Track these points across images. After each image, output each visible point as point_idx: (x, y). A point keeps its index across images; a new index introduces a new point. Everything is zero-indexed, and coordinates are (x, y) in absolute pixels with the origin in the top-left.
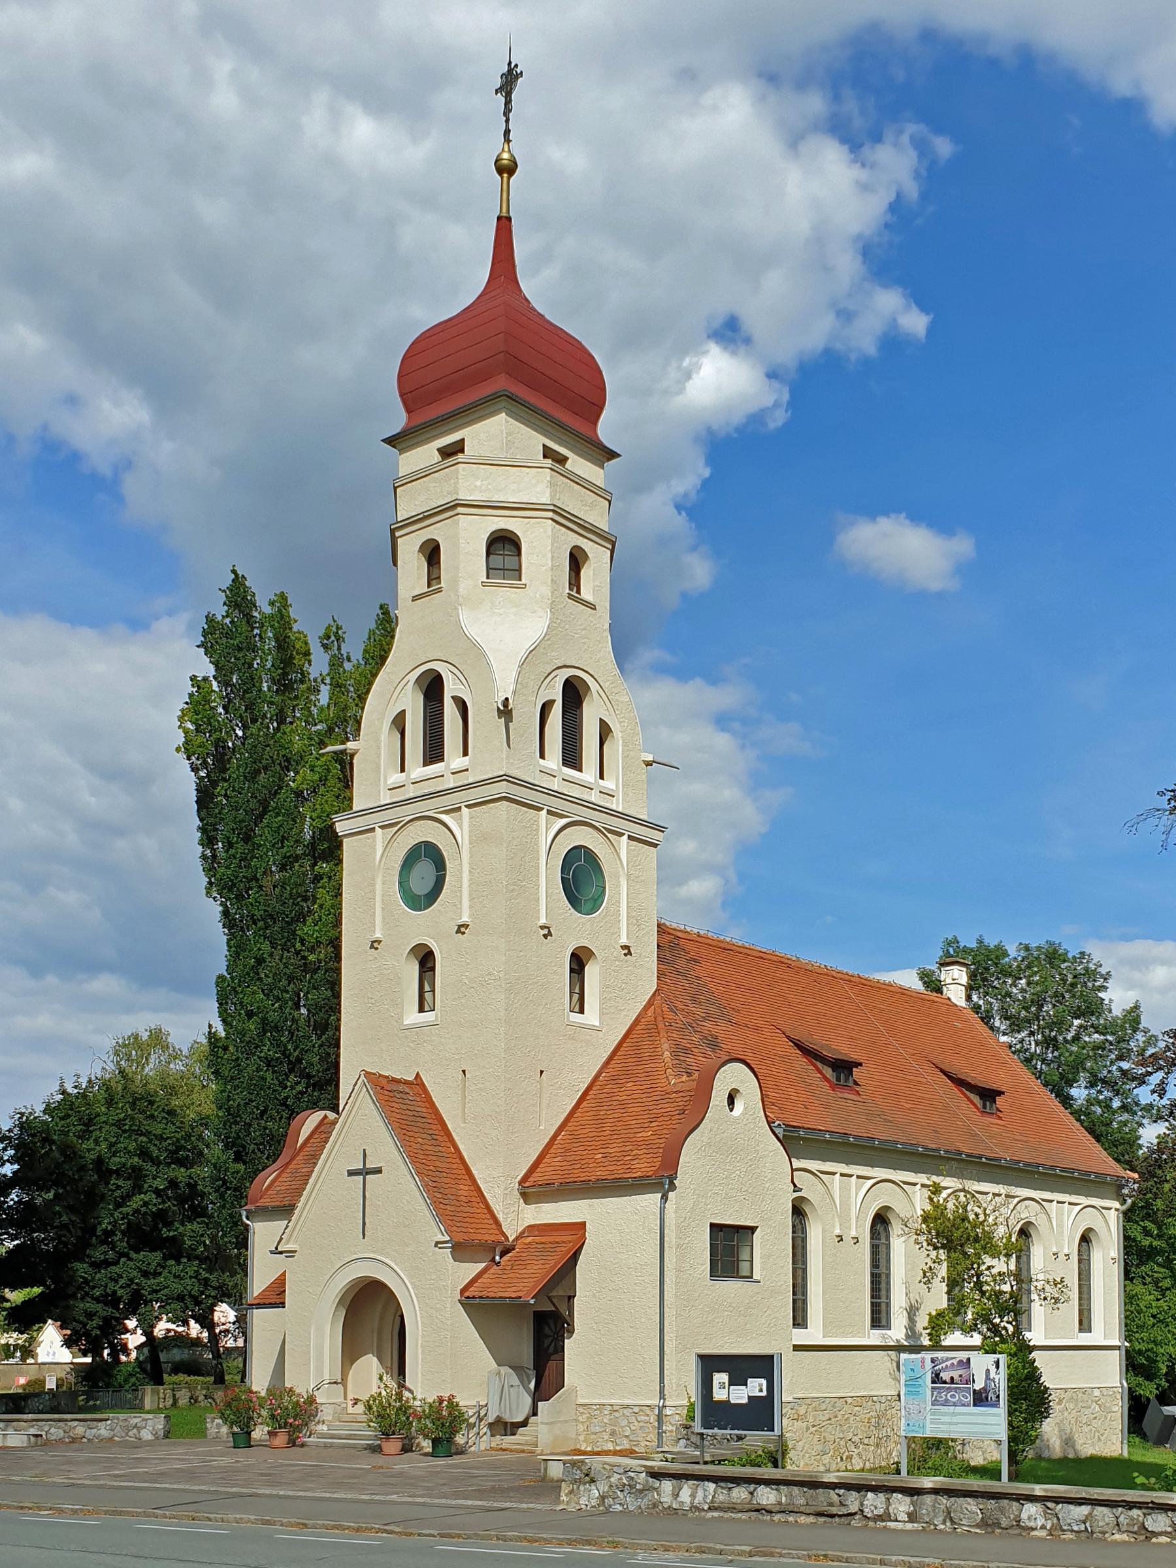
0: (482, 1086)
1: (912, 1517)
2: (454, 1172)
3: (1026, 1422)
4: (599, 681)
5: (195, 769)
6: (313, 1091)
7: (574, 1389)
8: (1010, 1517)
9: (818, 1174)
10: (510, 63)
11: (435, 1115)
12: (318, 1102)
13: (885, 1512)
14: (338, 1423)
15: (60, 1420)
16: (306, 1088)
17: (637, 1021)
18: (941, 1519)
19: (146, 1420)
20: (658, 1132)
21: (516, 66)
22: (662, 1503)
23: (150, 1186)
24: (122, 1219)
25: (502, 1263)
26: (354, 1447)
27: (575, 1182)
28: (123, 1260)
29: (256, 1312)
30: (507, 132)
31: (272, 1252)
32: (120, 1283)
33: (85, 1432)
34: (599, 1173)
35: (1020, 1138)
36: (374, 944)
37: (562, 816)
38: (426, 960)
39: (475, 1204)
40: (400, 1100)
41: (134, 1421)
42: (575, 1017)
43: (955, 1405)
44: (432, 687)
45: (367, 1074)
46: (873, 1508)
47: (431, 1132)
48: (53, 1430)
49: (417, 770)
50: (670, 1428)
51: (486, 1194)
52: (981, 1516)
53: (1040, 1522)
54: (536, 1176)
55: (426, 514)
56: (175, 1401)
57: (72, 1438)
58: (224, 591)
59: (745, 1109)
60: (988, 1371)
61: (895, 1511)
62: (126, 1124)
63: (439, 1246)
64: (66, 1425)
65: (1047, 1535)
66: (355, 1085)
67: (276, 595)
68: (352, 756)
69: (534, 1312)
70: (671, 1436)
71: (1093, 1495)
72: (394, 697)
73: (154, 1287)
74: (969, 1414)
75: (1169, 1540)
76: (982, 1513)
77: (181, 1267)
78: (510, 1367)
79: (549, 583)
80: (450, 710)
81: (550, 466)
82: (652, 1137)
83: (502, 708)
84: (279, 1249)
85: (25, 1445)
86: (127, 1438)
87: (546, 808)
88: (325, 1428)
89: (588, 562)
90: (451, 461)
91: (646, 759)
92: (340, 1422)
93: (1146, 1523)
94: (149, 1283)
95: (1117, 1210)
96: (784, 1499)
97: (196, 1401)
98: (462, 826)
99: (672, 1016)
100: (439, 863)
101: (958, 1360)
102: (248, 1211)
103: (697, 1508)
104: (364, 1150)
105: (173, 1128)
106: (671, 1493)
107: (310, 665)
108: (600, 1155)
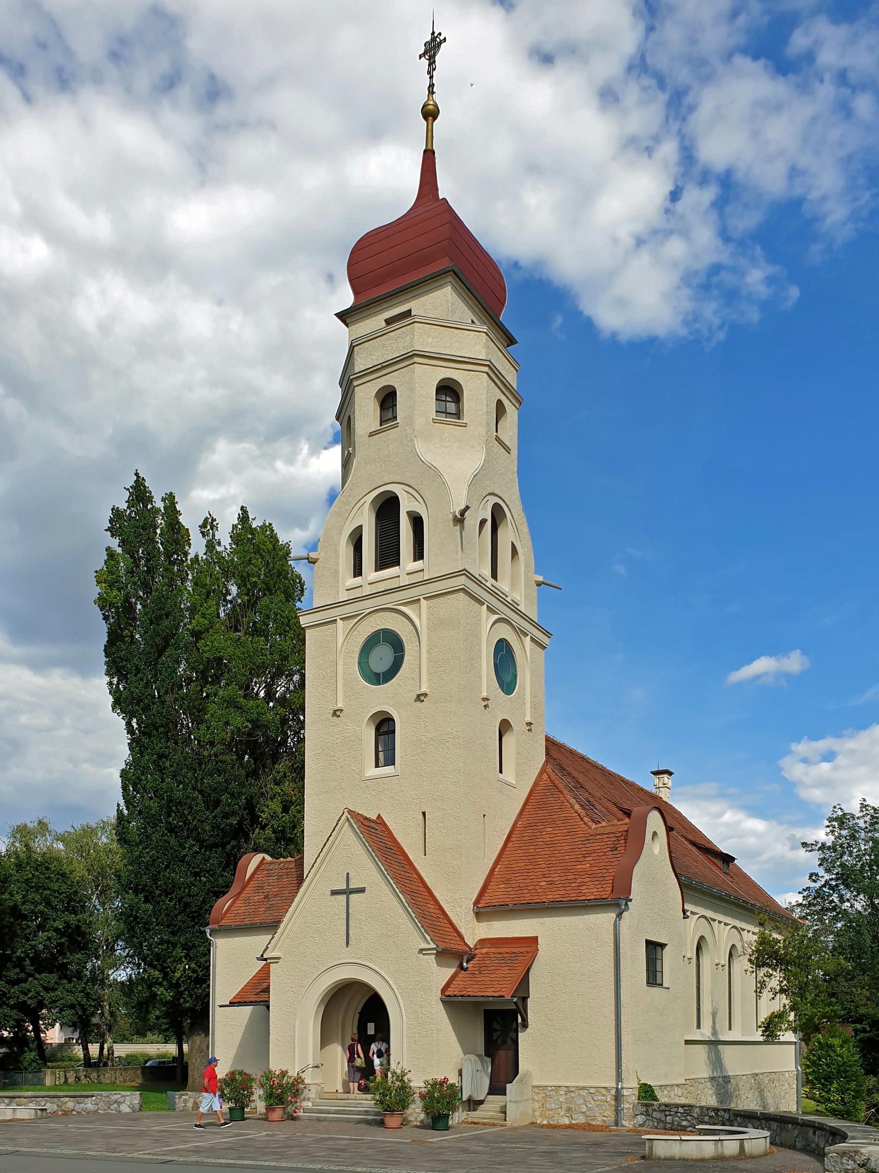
3: (853, 1099)
4: (512, 511)
5: (106, 618)
6: (205, 851)
7: (528, 1073)
10: (433, 33)
11: (398, 848)
12: (209, 859)
14: (319, 1100)
15: (54, 1097)
16: (200, 850)
17: (536, 784)
19: (125, 1096)
21: (440, 34)
23: (52, 926)
24: (30, 949)
26: (348, 1121)
27: (530, 903)
28: (30, 979)
30: (432, 86)
32: (30, 995)
33: (75, 1106)
36: (336, 713)
45: (350, 812)
49: (370, 572)
50: (627, 1106)
51: (448, 913)
54: (486, 899)
55: (384, 365)
56: (66, 1079)
58: (128, 489)
59: (660, 849)
62: (32, 882)
63: (424, 952)
64: (59, 1101)
66: (338, 821)
67: (166, 494)
69: (484, 1010)
70: (629, 1112)
72: (352, 515)
73: (53, 998)
77: (72, 985)
78: (475, 1055)
79: (485, 424)
81: (486, 331)
83: (459, 517)
85: (33, 1117)
86: (109, 1111)
88: (310, 1104)
89: (505, 415)
91: (538, 580)
92: (320, 1099)
94: (49, 995)
97: (79, 1080)
98: (421, 615)
100: (396, 644)
102: (211, 931)
104: (348, 874)
105: (65, 886)
107: (190, 547)
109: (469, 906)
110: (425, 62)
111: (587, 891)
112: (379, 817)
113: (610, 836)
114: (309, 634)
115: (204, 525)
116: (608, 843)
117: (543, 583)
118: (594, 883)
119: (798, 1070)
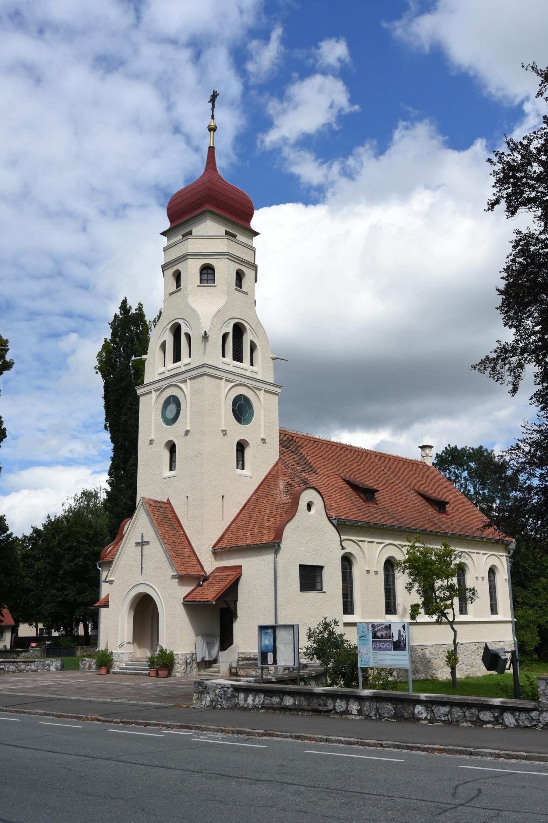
0: (195, 503)
1: (360, 712)
2: (182, 543)
8: (409, 712)
10: (214, 91)
13: (346, 710)
18: (374, 713)
20: (275, 523)
21: (216, 92)
22: (239, 704)
25: (204, 585)
34: (247, 542)
35: (457, 523)
37: (232, 382)
38: (172, 448)
39: (191, 558)
40: (159, 511)
41: (48, 662)
42: (240, 471)
43: (384, 650)
44: (176, 330)
46: (340, 707)
47: (172, 525)
48: (11, 667)
52: (394, 712)
53: (424, 715)
54: (221, 545)
60: (400, 631)
61: (351, 709)
65: (428, 723)
68: (145, 361)
71: (451, 700)
74: (392, 655)
75: (492, 726)
76: (395, 710)
80: (183, 339)
82: (272, 525)
87: (224, 378)
90: (186, 238)
93: (480, 716)
95: (506, 556)
96: (297, 702)
98: (187, 388)
99: (286, 470)
101: (384, 626)
103: (255, 707)
104: (142, 533)
108: (249, 534)
109: (208, 549)
110: (211, 104)
112: (168, 500)
114: (142, 400)
115: (495, 195)
117: (276, 358)
119: (514, 641)
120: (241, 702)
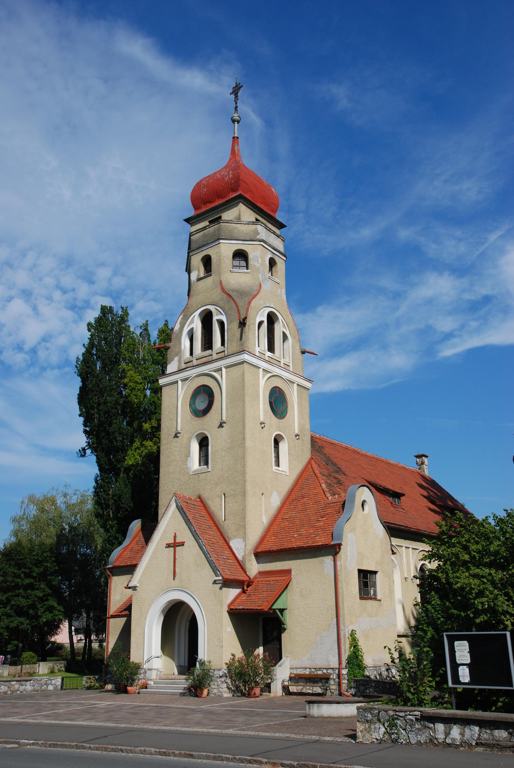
9: (396, 546)
21: (240, 84)
29: (112, 620)
31: (126, 588)
33: (19, 688)
47: (208, 524)
57: (12, 691)
84: (129, 586)
106: (443, 731)
110: (233, 96)
111: (319, 539)
113: (337, 504)
116: (336, 508)
118: (324, 534)
120: (441, 736)
